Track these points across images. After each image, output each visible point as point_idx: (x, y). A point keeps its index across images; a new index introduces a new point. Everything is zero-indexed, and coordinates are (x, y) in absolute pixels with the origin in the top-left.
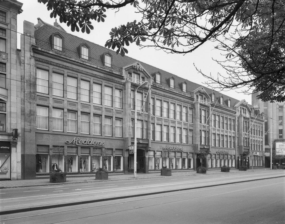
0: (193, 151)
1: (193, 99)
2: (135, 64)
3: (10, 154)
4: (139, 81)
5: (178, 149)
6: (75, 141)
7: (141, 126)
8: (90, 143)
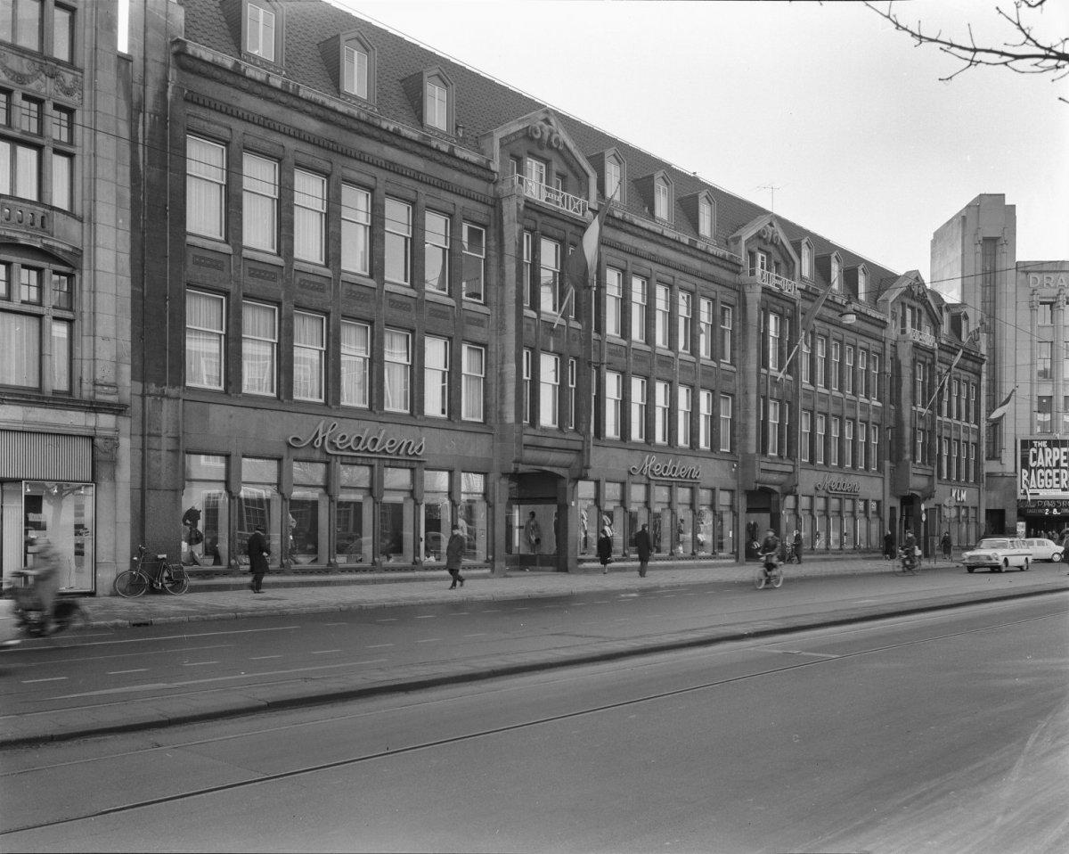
0: (732, 484)
1: (735, 268)
2: (536, 119)
3: (554, 508)
4: (548, 190)
5: (387, 446)
6: (324, 438)
7: (478, 369)
8: (374, 447)
